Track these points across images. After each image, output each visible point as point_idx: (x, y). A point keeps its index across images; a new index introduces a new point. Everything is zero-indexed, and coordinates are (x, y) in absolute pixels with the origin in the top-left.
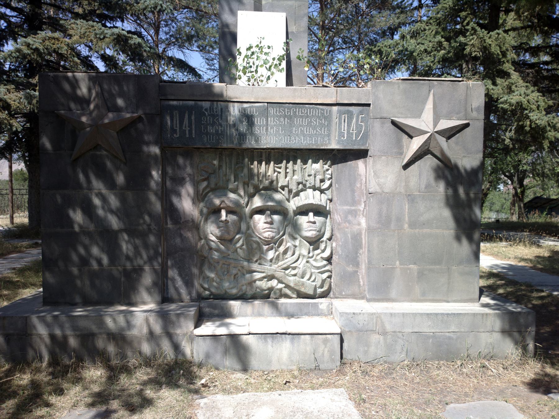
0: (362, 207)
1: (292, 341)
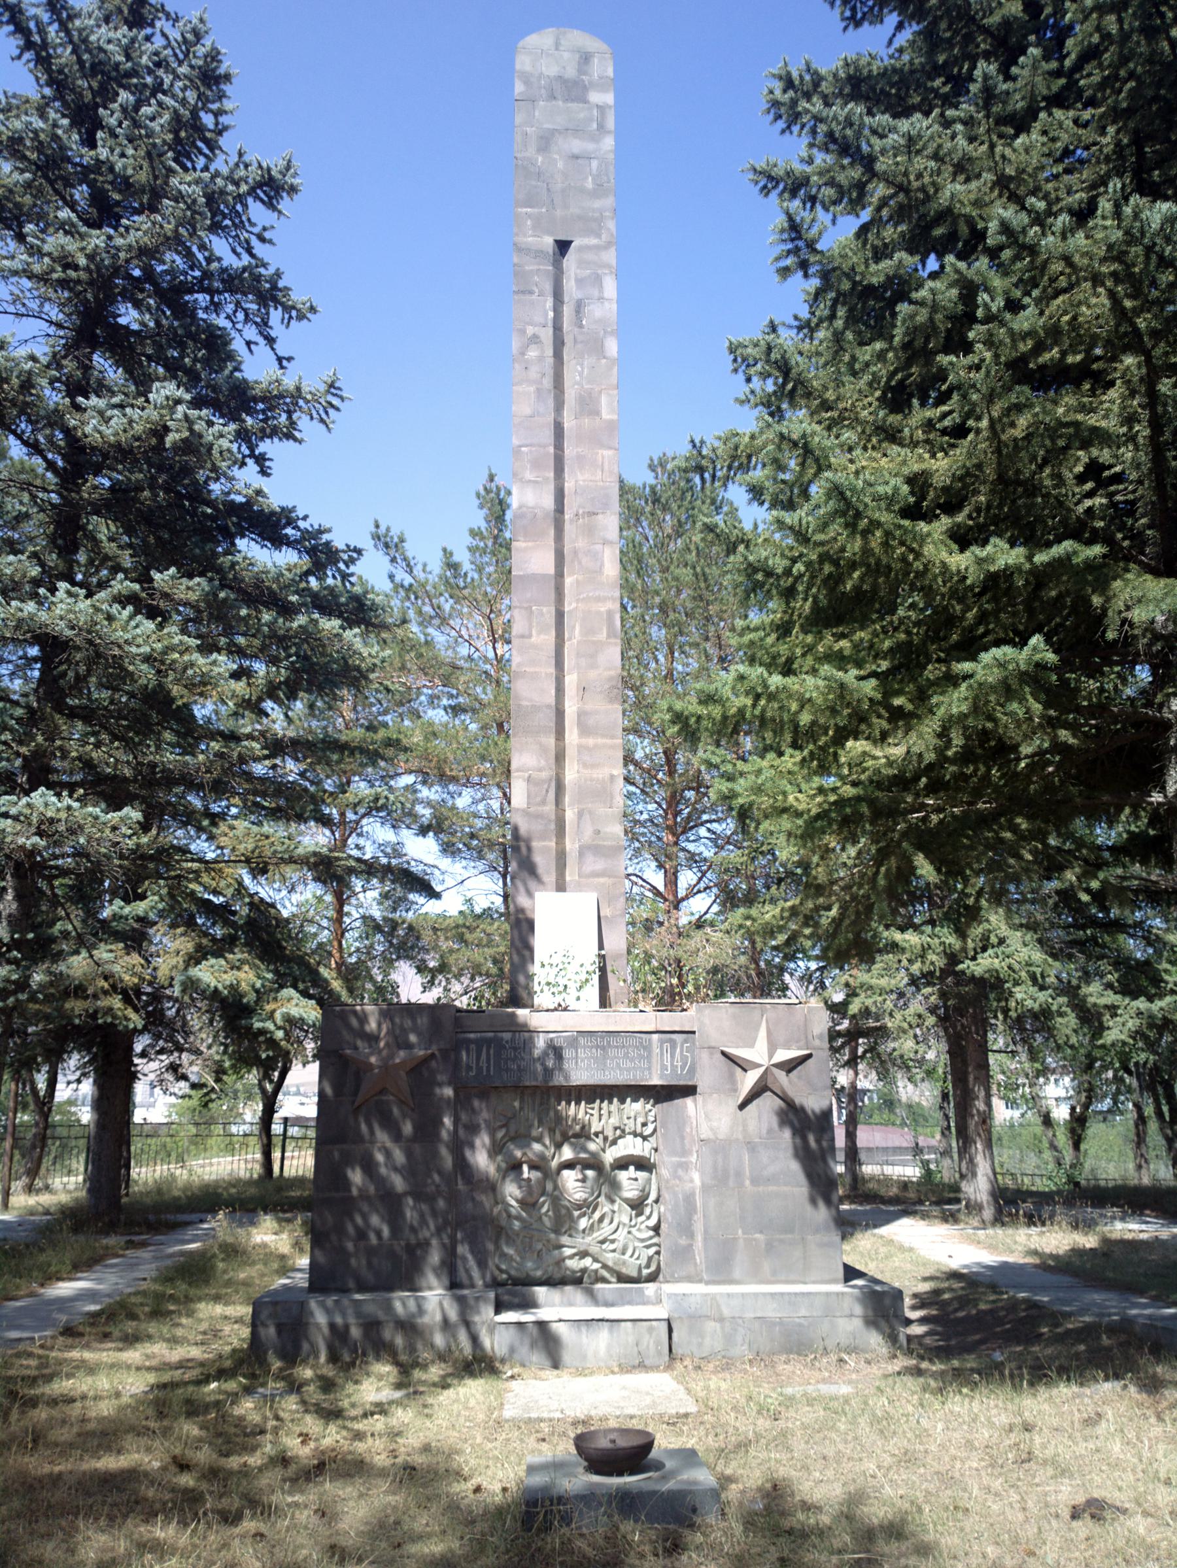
0: (693, 1159)
1: (611, 1330)
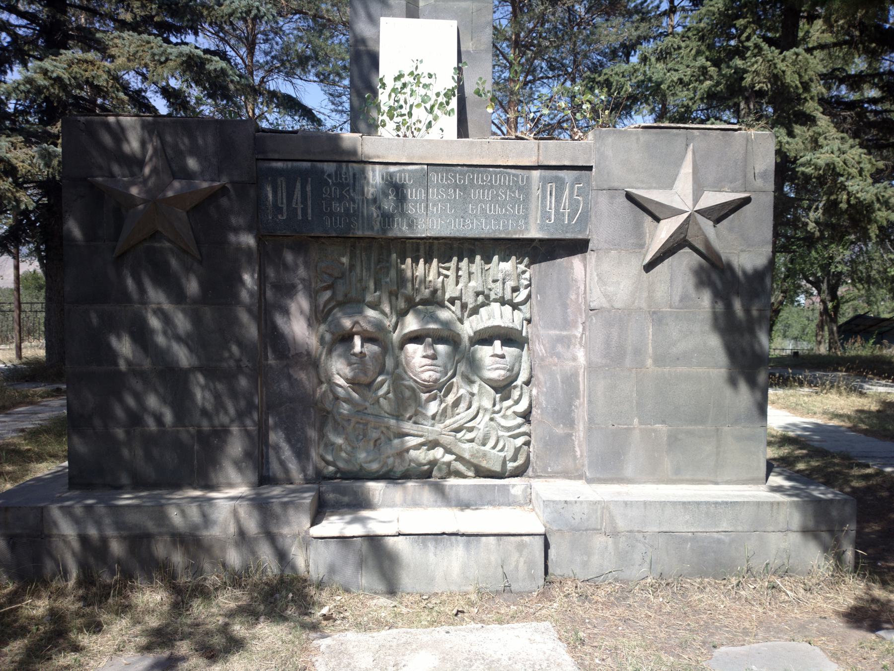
0: (578, 331)
1: (467, 546)
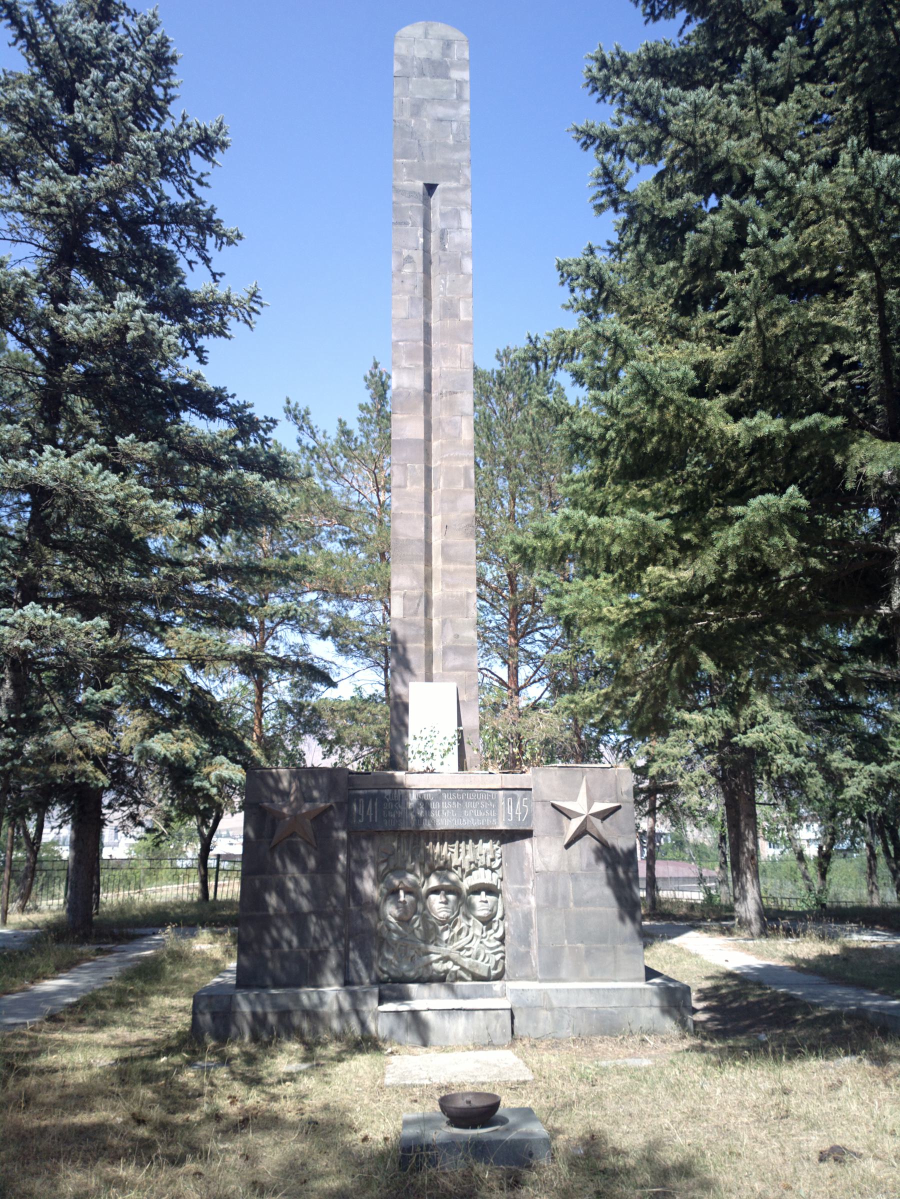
0: (530, 886)
1: (467, 1018)
